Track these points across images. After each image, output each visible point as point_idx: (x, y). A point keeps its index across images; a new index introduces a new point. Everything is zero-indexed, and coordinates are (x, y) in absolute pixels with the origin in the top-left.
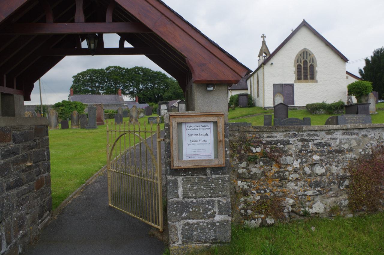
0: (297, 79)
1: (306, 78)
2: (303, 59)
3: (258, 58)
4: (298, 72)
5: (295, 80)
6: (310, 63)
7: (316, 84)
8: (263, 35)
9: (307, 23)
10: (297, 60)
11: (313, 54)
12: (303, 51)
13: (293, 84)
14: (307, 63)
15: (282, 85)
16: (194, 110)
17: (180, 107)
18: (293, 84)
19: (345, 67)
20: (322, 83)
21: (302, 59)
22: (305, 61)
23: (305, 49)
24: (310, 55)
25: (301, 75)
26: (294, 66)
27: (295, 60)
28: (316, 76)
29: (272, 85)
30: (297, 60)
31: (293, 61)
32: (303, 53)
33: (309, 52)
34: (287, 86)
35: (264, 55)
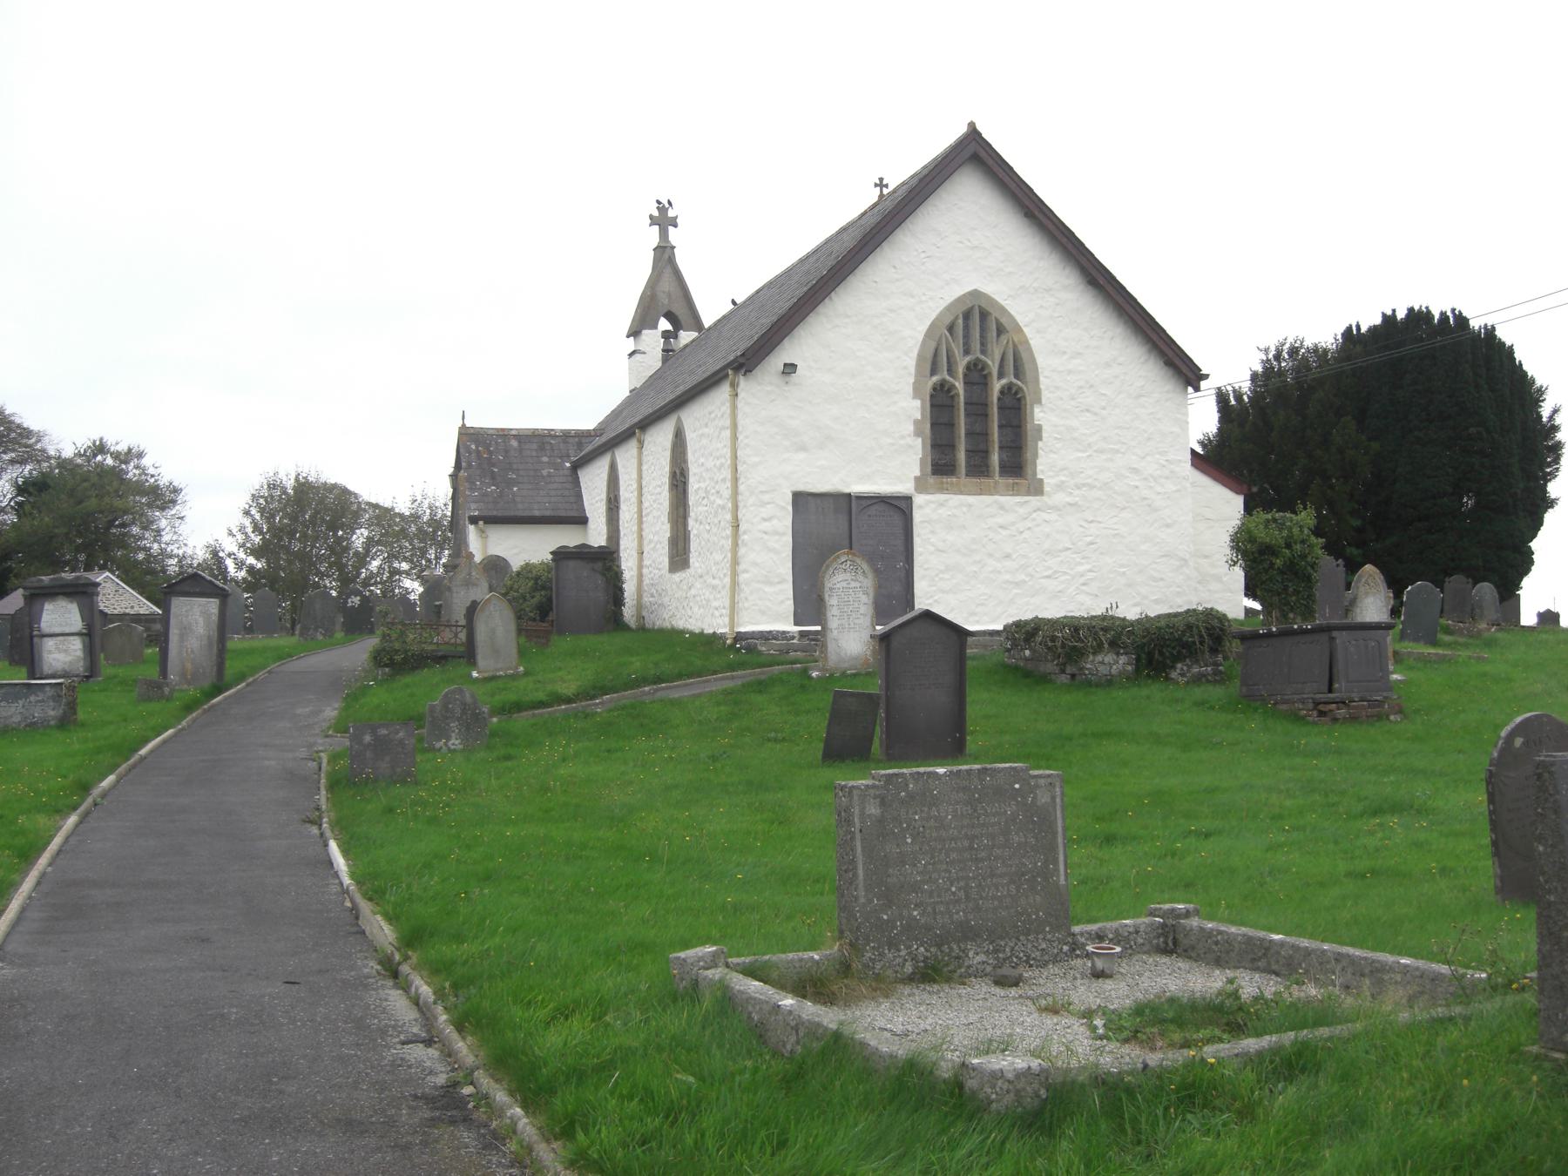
0: (929, 469)
1: (978, 467)
2: (967, 352)
3: (630, 344)
4: (934, 425)
5: (918, 473)
6: (1004, 381)
7: (1034, 501)
8: (881, 179)
9: (987, 146)
10: (929, 355)
11: (1019, 330)
12: (965, 308)
13: (908, 499)
14: (985, 377)
15: (845, 503)
16: (1000, 476)
17: (173, 621)
18: (908, 499)
19: (1186, 414)
20: (1069, 499)
21: (958, 352)
22: (975, 365)
23: (975, 294)
24: (1001, 330)
25: (952, 447)
26: (917, 393)
27: (921, 358)
28: (1036, 455)
29: (789, 498)
30: (934, 359)
31: (911, 362)
32: (967, 316)
33: (995, 314)
34: (873, 510)
35: (664, 325)
